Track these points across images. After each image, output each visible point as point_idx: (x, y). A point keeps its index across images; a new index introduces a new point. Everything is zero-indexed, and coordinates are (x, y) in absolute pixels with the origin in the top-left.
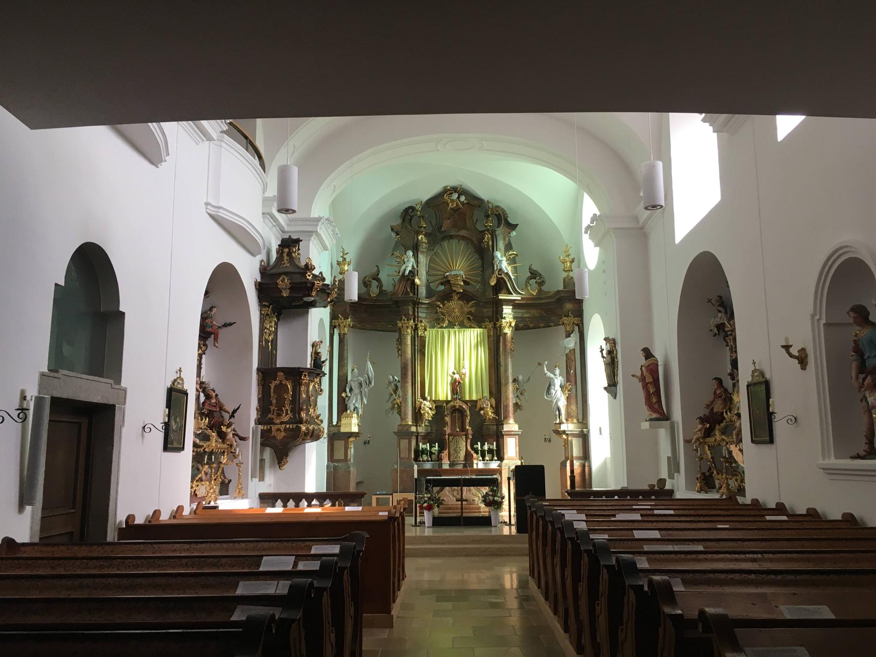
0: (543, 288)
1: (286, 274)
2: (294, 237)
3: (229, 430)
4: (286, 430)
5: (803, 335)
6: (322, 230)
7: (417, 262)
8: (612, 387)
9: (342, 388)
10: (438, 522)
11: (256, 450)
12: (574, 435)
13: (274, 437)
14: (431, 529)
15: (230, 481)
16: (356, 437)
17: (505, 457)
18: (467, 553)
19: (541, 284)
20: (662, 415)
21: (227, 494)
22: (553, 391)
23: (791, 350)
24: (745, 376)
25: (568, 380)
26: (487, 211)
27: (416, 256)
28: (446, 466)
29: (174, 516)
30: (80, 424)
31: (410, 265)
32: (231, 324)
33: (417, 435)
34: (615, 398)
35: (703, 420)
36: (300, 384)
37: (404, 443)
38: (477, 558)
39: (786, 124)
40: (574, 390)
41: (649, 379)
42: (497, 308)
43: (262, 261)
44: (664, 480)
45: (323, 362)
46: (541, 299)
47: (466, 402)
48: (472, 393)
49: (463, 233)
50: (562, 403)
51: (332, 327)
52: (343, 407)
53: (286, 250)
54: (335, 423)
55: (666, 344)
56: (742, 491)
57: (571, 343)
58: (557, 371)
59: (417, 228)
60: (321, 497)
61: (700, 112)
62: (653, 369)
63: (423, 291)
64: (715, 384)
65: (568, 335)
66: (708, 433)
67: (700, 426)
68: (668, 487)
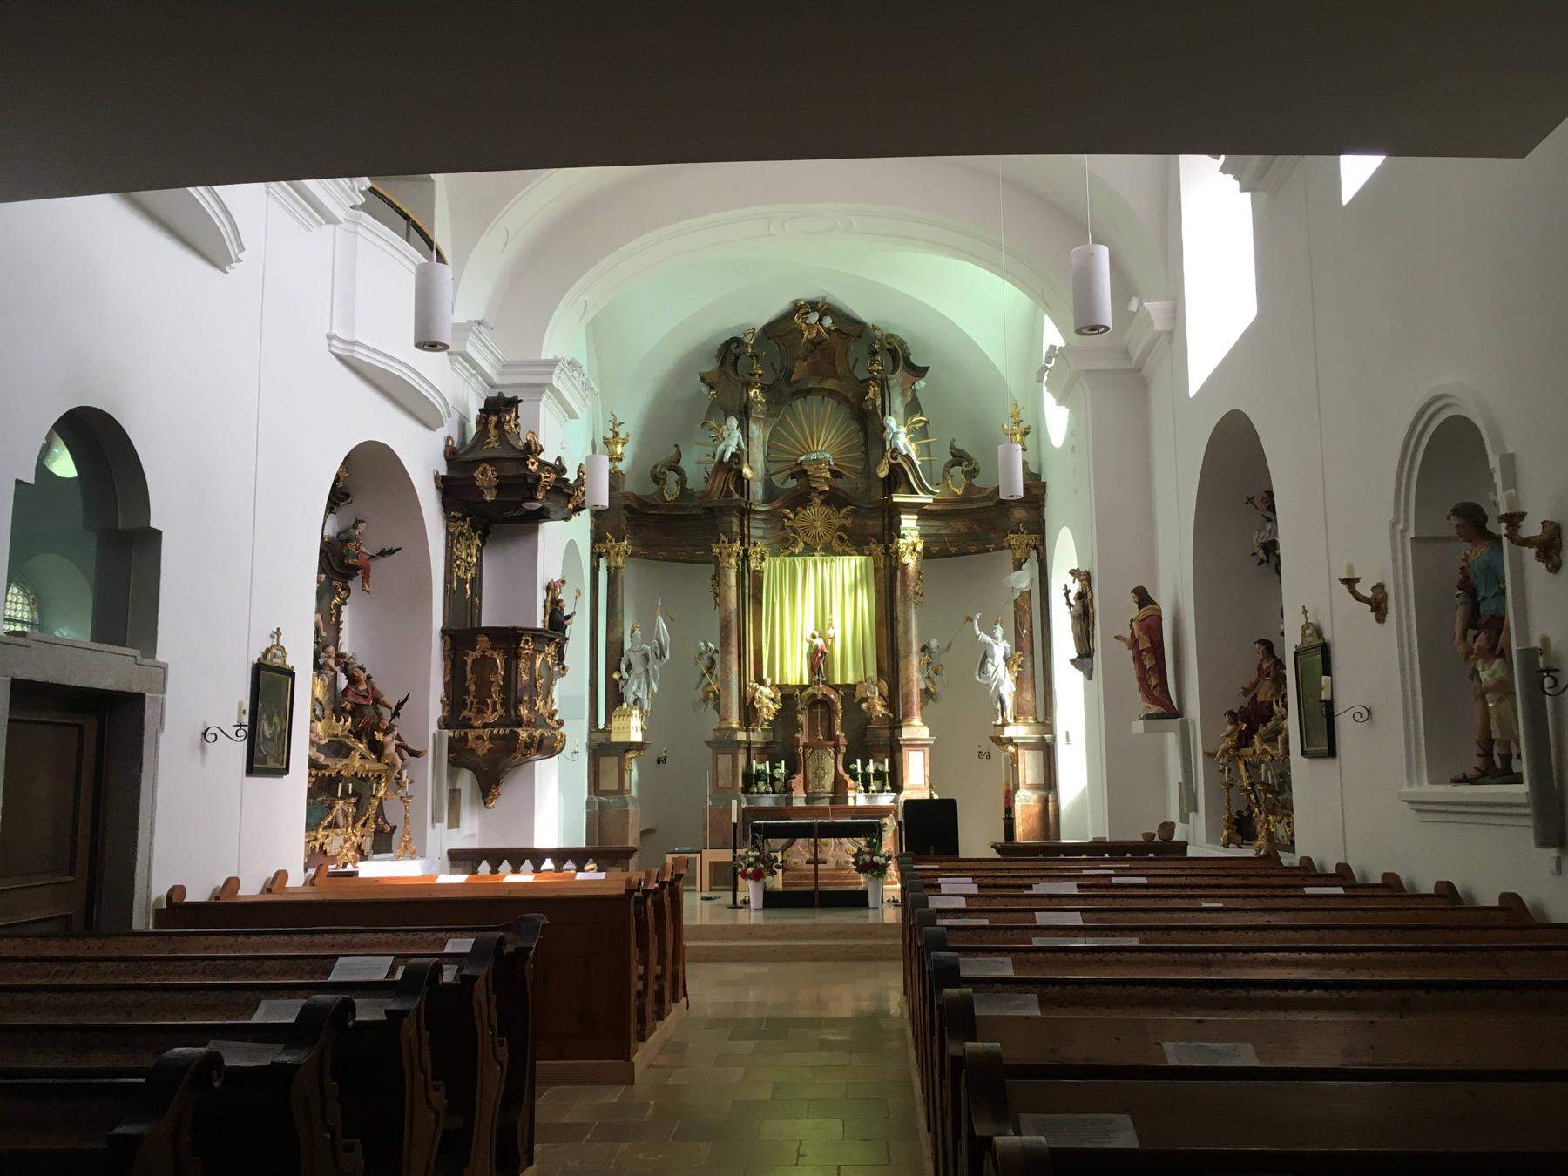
0: (975, 482)
1: (490, 461)
2: (508, 395)
3: (389, 738)
4: (492, 738)
5: (1379, 562)
6: (559, 380)
7: (747, 436)
8: (1084, 658)
9: (613, 666)
10: (772, 900)
11: (439, 773)
12: (1028, 746)
13: (472, 750)
14: (761, 914)
15: (394, 828)
16: (639, 750)
17: (906, 785)
18: (816, 956)
19: (971, 474)
20: (1167, 710)
21: (389, 850)
22: (990, 668)
23: (1358, 587)
24: (1292, 640)
25: (1018, 647)
26: (871, 345)
27: (744, 427)
28: (799, 800)
29: (268, 889)
30: (80, 727)
31: (734, 444)
32: (392, 552)
33: (748, 746)
34: (1090, 678)
35: (1234, 717)
36: (518, 657)
37: (724, 761)
38: (832, 964)
39: (1357, 171)
40: (1028, 664)
41: (1144, 644)
42: (891, 518)
43: (449, 438)
44: (1172, 825)
45: (568, 617)
46: (971, 501)
47: (835, 688)
48: (846, 671)
49: (830, 384)
50: (1008, 689)
51: (596, 556)
52: (616, 698)
53: (494, 419)
54: (601, 726)
55: (1175, 584)
56: (1291, 846)
57: (1024, 580)
58: (999, 631)
59: (747, 377)
60: (578, 857)
61: (1214, 152)
62: (1151, 627)
63: (757, 490)
64: (1259, 649)
65: (1018, 566)
66: (1244, 740)
67: (1230, 728)
68: (1178, 837)
